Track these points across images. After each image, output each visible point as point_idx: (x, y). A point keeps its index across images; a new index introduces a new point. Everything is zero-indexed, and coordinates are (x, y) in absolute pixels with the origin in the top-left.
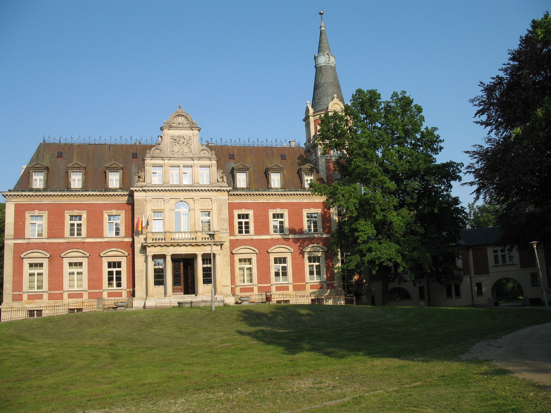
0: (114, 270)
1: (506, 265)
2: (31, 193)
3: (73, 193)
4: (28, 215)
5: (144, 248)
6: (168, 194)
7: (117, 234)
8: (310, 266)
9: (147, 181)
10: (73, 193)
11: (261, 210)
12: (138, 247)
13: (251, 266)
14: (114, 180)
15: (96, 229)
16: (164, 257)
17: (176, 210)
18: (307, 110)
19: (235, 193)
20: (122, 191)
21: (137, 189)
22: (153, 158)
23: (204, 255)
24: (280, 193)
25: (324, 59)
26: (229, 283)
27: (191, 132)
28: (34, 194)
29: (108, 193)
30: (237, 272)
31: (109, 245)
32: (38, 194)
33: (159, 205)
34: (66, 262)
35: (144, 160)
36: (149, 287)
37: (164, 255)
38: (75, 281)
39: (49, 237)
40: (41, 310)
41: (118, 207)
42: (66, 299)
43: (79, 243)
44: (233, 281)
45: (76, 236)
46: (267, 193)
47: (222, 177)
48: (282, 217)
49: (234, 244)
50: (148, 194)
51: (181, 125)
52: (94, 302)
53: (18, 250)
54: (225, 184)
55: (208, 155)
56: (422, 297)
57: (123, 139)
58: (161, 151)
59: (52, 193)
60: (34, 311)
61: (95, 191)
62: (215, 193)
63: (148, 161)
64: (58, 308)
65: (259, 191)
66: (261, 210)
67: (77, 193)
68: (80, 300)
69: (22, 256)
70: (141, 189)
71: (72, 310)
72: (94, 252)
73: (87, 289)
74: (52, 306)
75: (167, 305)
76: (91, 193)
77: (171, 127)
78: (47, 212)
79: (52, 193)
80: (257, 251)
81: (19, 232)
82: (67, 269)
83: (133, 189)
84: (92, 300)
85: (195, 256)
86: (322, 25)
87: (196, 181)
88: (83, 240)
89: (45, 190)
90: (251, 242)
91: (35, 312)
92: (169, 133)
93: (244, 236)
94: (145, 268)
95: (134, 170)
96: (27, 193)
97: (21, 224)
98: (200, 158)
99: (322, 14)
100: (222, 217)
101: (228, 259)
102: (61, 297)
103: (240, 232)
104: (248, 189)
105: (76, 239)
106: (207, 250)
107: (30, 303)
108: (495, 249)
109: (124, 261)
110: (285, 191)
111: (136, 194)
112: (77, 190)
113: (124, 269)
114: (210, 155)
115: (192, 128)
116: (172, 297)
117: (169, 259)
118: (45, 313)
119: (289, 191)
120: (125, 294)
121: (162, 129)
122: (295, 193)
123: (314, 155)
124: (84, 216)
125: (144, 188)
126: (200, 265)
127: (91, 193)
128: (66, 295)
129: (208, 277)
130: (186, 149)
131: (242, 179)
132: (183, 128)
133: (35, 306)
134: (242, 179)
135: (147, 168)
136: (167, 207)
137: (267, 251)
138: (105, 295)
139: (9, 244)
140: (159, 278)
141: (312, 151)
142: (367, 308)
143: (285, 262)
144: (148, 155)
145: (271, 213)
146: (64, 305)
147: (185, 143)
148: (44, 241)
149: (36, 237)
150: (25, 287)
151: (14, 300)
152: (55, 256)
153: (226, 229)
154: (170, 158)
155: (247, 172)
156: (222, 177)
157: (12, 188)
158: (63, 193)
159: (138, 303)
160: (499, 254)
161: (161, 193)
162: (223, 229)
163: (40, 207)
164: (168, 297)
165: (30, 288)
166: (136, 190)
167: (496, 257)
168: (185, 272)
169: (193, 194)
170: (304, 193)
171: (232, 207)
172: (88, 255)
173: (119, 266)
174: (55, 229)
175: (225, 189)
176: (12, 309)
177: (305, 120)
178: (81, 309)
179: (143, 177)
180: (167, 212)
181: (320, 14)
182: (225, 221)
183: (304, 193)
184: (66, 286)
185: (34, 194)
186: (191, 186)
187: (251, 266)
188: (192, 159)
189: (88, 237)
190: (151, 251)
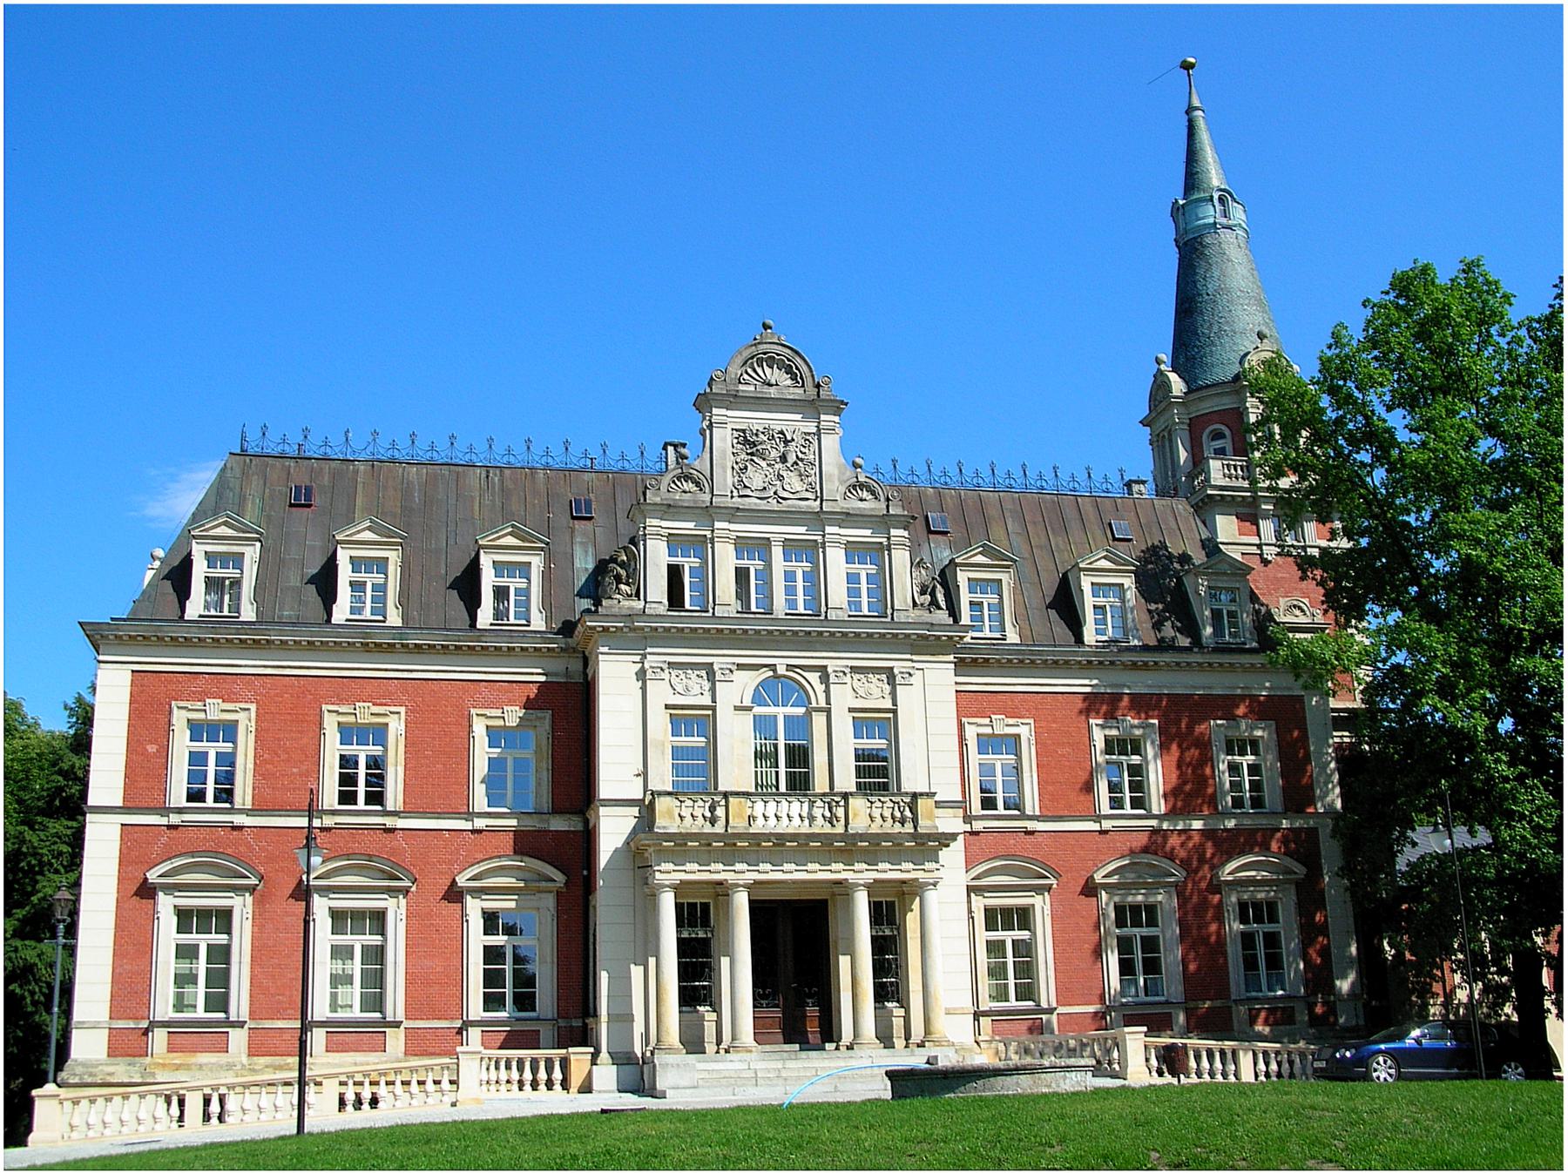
13: (221, 939)
18: (1160, 384)
36: (738, 1002)
37: (720, 883)
45: (361, 804)
57: (537, 450)
69: (152, 876)
77: (735, 400)
84: (262, 1061)
86: (1196, 103)
88: (389, 822)
92: (729, 422)
97: (152, 749)
98: (848, 518)
99: (1192, 66)
106: (888, 872)
116: (754, 1055)
117: (741, 901)
121: (703, 403)
124: (396, 727)
130: (794, 482)
147: (792, 458)
148: (239, 820)
150: (164, 1007)
154: (734, 514)
165: (180, 1005)
181: (1187, 66)
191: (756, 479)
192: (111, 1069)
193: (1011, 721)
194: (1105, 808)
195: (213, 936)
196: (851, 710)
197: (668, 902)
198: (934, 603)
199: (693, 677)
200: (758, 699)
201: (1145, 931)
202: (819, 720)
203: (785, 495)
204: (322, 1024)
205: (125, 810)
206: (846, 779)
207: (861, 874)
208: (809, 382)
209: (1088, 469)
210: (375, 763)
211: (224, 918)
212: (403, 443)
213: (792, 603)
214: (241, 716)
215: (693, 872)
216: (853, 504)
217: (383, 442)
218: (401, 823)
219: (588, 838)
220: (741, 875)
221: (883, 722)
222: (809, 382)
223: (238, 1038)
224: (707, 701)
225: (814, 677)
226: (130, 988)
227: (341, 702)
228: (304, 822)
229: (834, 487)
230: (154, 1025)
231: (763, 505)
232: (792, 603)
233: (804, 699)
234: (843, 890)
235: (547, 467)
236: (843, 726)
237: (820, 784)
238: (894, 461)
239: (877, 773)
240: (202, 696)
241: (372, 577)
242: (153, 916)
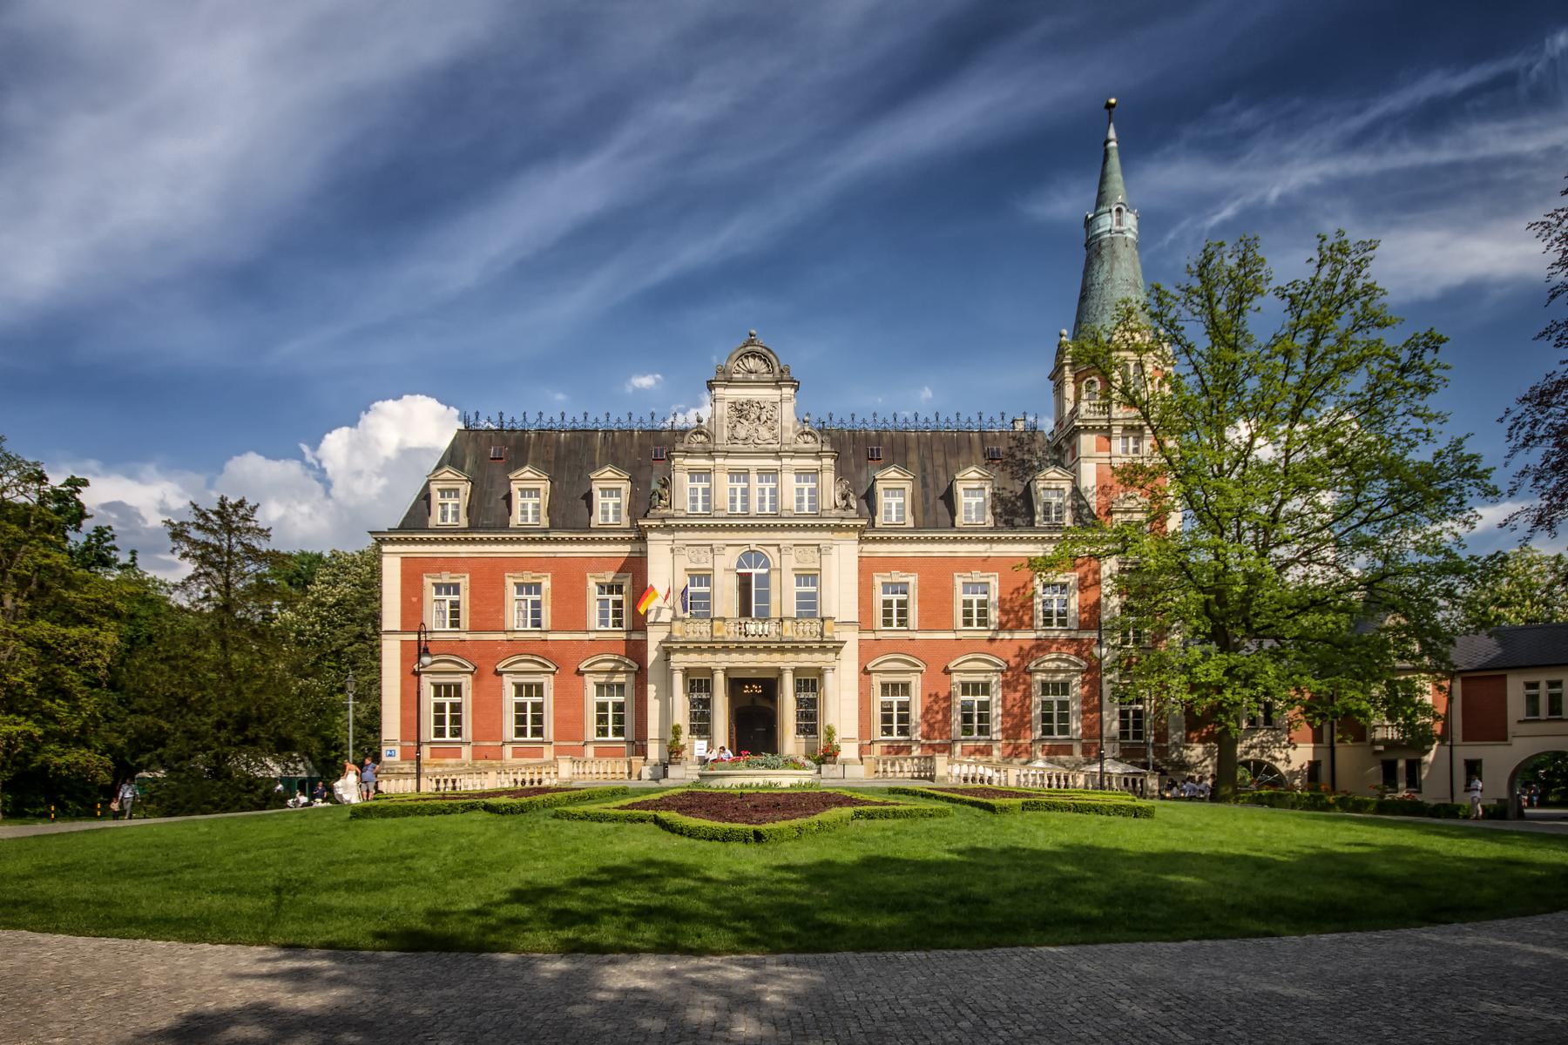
1: (1539, 721)
7: (455, 624)
11: (937, 576)
13: (906, 698)
22: (689, 453)
31: (518, 648)
39: (471, 631)
45: (975, 626)
51: (753, 377)
57: (635, 419)
62: (828, 535)
66: (937, 576)
73: (551, 738)
77: (730, 382)
80: (923, 668)
83: (646, 523)
88: (543, 636)
93: (894, 633)
98: (797, 453)
103: (888, 623)
106: (806, 660)
108: (1532, 678)
115: (777, 384)
117: (720, 678)
123: (1069, 455)
124: (546, 584)
130: (764, 432)
132: (760, 384)
141: (1065, 445)
142: (412, 701)
144: (679, 447)
147: (763, 418)
148: (463, 636)
149: (529, 627)
154: (727, 454)
157: (396, 524)
160: (1543, 692)
167: (1532, 701)
171: (866, 568)
177: (1052, 378)
188: (778, 455)
190: (679, 661)
194: (960, 625)
197: (678, 678)
198: (848, 506)
200: (740, 565)
202: (774, 577)
205: (402, 632)
206: (791, 609)
207: (788, 662)
208: (777, 370)
210: (902, 604)
211: (539, 690)
212: (557, 419)
213: (762, 508)
215: (694, 660)
216: (801, 445)
217: (880, 420)
218: (550, 637)
219: (643, 644)
220: (720, 662)
221: (808, 577)
222: (777, 370)
224: (709, 566)
225: (773, 550)
227: (515, 571)
228: (415, 637)
229: (790, 435)
232: (762, 508)
233: (766, 565)
234: (780, 671)
235: (620, 430)
236: (790, 580)
237: (774, 613)
238: (563, 414)
239: (809, 606)
240: (440, 570)
241: (529, 494)
242: (584, 686)
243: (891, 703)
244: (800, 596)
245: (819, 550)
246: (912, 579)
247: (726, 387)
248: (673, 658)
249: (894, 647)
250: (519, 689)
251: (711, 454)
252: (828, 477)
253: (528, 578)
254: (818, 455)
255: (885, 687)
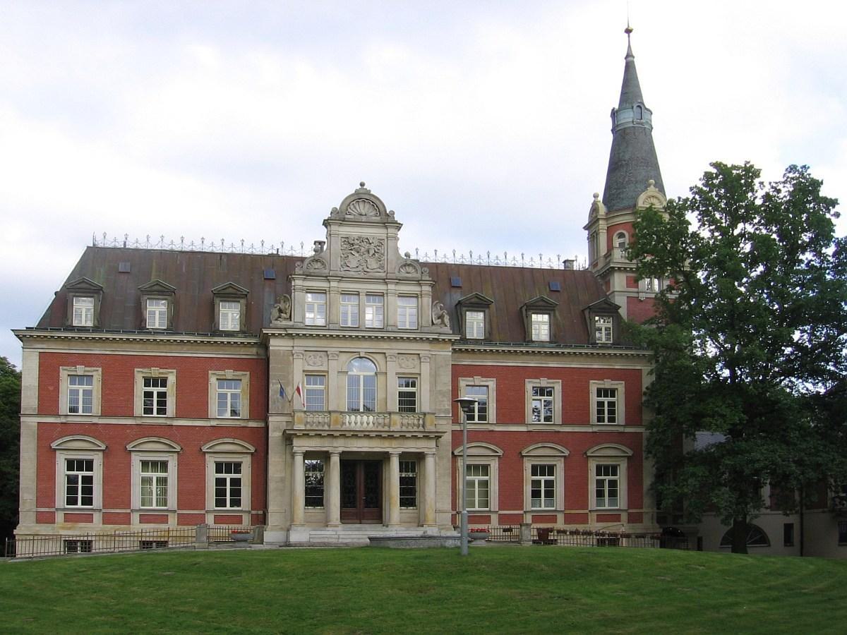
0: (228, 477)
2: (70, 335)
3: (151, 338)
4: (64, 373)
5: (288, 438)
6: (336, 343)
8: (533, 482)
9: (297, 317)
10: (151, 338)
12: (275, 435)
13: (486, 478)
14: (230, 317)
15: (194, 402)
16: (326, 456)
17: (349, 373)
19: (464, 347)
20: (246, 337)
21: (277, 332)
22: (307, 276)
23: (403, 456)
24: (548, 350)
25: (631, 114)
26: (447, 505)
27: (384, 231)
28: (76, 335)
29: (216, 339)
30: (460, 486)
31: (219, 432)
32: (83, 335)
33: (317, 364)
34: (136, 460)
35: (289, 281)
37: (327, 452)
38: (152, 490)
39: (104, 415)
40: (91, 542)
41: (238, 364)
42: (136, 525)
43: (160, 426)
44: (454, 506)
46: (524, 350)
47: (441, 317)
48: (550, 394)
49: (457, 438)
50: (297, 342)
52: (190, 530)
53: (46, 435)
54: (448, 329)
55: (415, 275)
56: (788, 540)
58: (323, 264)
59: (110, 336)
60: (76, 542)
61: (194, 335)
62: (426, 346)
63: (298, 283)
64: (121, 539)
65: (508, 345)
67: (159, 338)
68: (163, 526)
69: (54, 445)
70: (283, 332)
71: (146, 545)
72: (191, 447)
73: (175, 507)
74: (111, 536)
75: (330, 540)
76: (186, 338)
78: (100, 369)
79: (110, 336)
80: (500, 453)
81: (48, 401)
82: (137, 473)
85: (386, 456)
87: (391, 322)
88: (169, 422)
89: (96, 329)
90: (488, 436)
91: (79, 544)
94: (288, 476)
95: (268, 298)
96: (63, 335)
97: (51, 388)
98: (399, 281)
100: (438, 388)
101: (447, 463)
102: (126, 520)
104: (488, 340)
105: (155, 418)
106: (412, 447)
107: (70, 529)
109: (246, 463)
110: (558, 346)
111: (273, 342)
112: (156, 332)
113: (245, 475)
114: (418, 276)
116: (340, 528)
117: (335, 460)
118: (98, 546)
119: (566, 347)
120: (246, 519)
122: (578, 351)
124: (172, 379)
125: (290, 331)
126: (393, 475)
127: (186, 338)
128: (135, 518)
129: (409, 495)
130: (373, 264)
131: (475, 323)
132: (371, 224)
133: (78, 533)
134: (475, 323)
135: (297, 295)
136: (334, 366)
137: (521, 453)
138: (210, 519)
139: (29, 424)
140: (315, 496)
143: (551, 473)
145: (529, 385)
146: (132, 535)
147: (372, 252)
148: (95, 420)
151: (39, 521)
152: (117, 446)
153: (446, 411)
154: (341, 279)
155: (487, 311)
156: (441, 317)
157: (34, 325)
158: (131, 337)
159: (272, 536)
161: (323, 343)
162: (440, 410)
163: (86, 360)
164: (335, 531)
166: (273, 334)
168: (363, 484)
169: (384, 346)
170: (595, 352)
172: (178, 449)
173: (90, 468)
174: (116, 400)
175: (446, 338)
176: (34, 537)
178: (166, 542)
179: (288, 311)
180: (333, 376)
182: (444, 396)
183: (595, 352)
184: (136, 502)
185: (76, 335)
186: (380, 330)
187: (486, 478)
188: (385, 281)
189: (178, 417)
190: (301, 445)
191: (353, 262)
192: (38, 529)
193: (484, 379)
195: (233, 475)
196: (397, 374)
198: (443, 322)
199: (410, 360)
201: (611, 478)
203: (368, 270)
204: (137, 511)
206: (394, 405)
209: (471, 252)
210: (611, 404)
214: (94, 373)
216: (403, 274)
223: (97, 517)
226: (45, 496)
227: (144, 367)
230: (207, 512)
231: (356, 275)
240: (74, 365)
243: (540, 482)
244: (401, 394)
245: (420, 358)
246: (492, 383)
247: (341, 225)
248: (296, 442)
249: (475, 436)
250: (70, 465)
251: (327, 278)
252: (427, 301)
253: (155, 372)
254: (419, 282)
255: (599, 469)
